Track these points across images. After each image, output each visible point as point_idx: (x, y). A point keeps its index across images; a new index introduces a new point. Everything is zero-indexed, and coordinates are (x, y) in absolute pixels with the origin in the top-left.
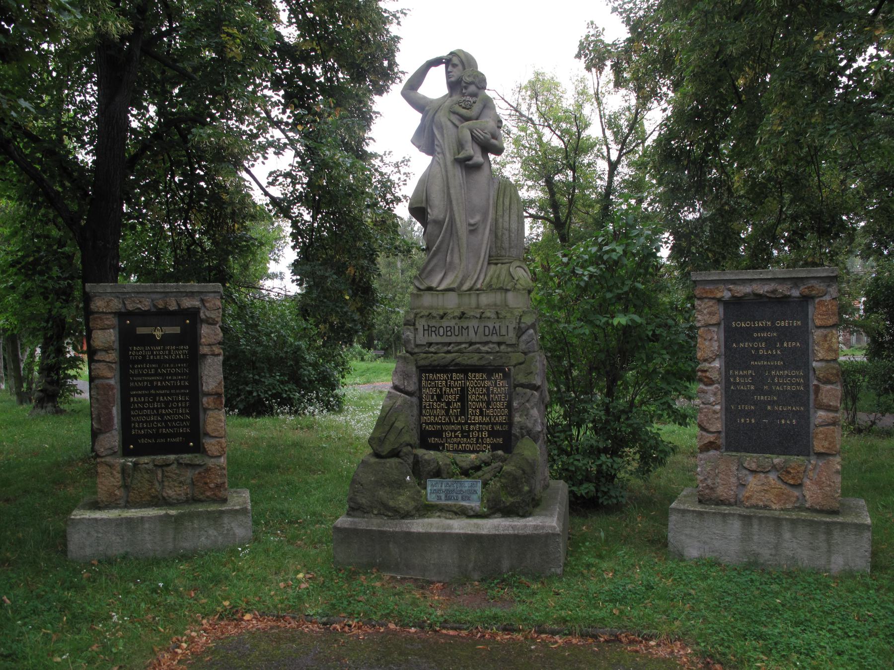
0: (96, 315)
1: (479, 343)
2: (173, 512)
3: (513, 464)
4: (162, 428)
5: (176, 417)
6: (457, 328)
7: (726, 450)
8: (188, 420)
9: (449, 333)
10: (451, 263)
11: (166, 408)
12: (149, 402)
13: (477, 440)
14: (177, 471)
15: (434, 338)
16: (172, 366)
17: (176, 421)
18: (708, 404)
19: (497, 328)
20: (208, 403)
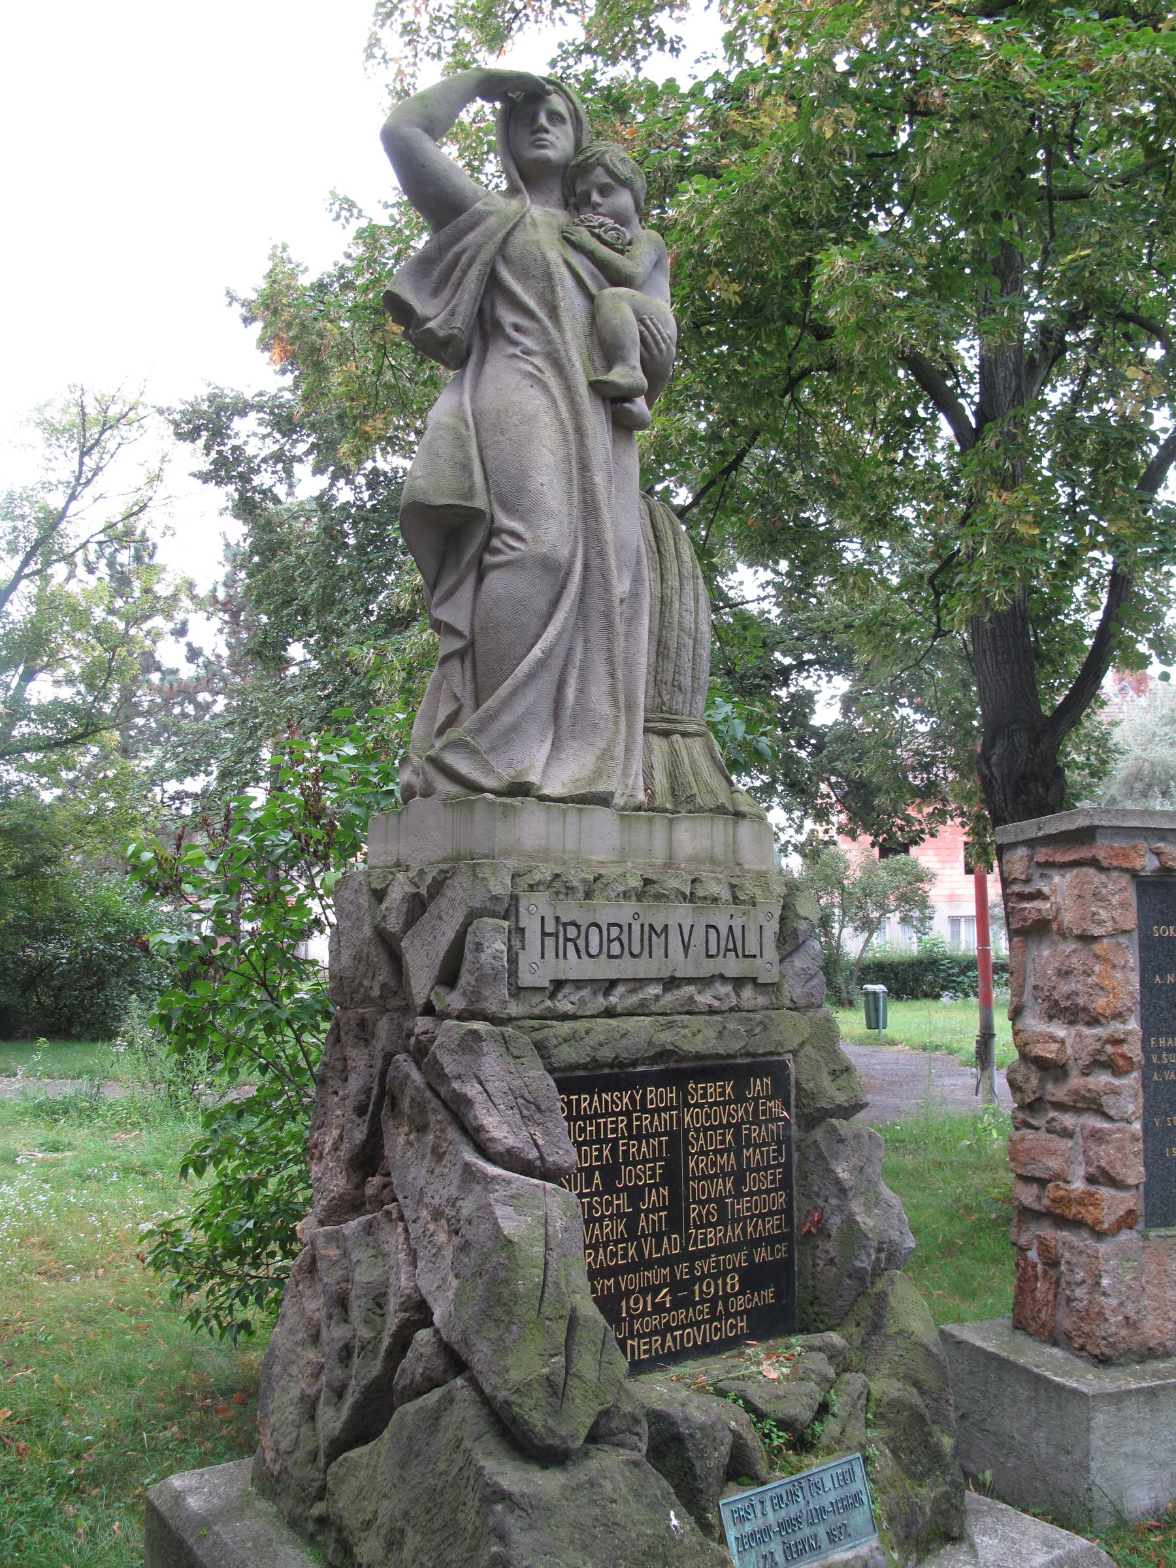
1: (690, 981)
3: (885, 1369)
6: (636, 928)
7: (1149, 1224)
9: (616, 949)
10: (582, 708)
13: (713, 1310)
15: (574, 967)
18: (1122, 1119)
19: (738, 932)
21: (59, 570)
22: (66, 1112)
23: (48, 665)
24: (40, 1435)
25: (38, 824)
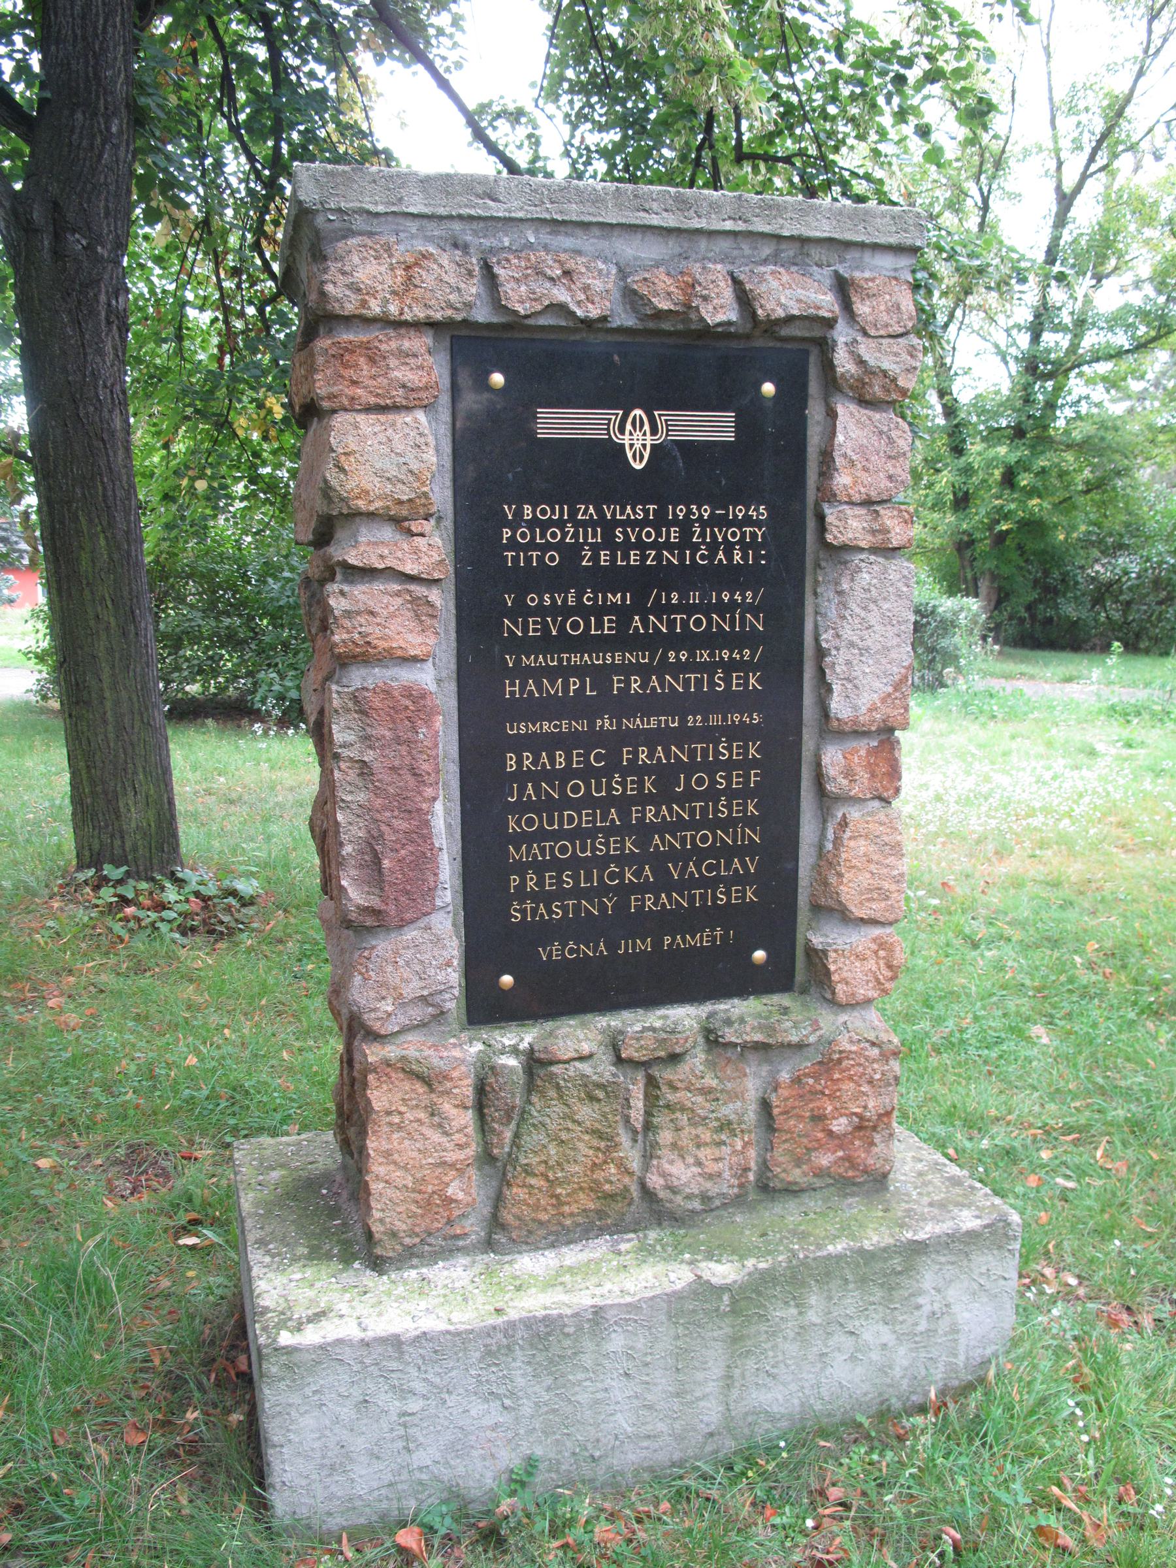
0: (347, 336)
2: (723, 1272)
4: (643, 888)
5: (705, 838)
8: (750, 849)
11: (664, 796)
12: (587, 773)
14: (710, 1081)
16: (694, 598)
17: (700, 855)
20: (849, 773)
21: (1125, 162)
22: (1138, 714)
23: (1116, 269)
24: (1124, 967)
25: (1109, 436)
